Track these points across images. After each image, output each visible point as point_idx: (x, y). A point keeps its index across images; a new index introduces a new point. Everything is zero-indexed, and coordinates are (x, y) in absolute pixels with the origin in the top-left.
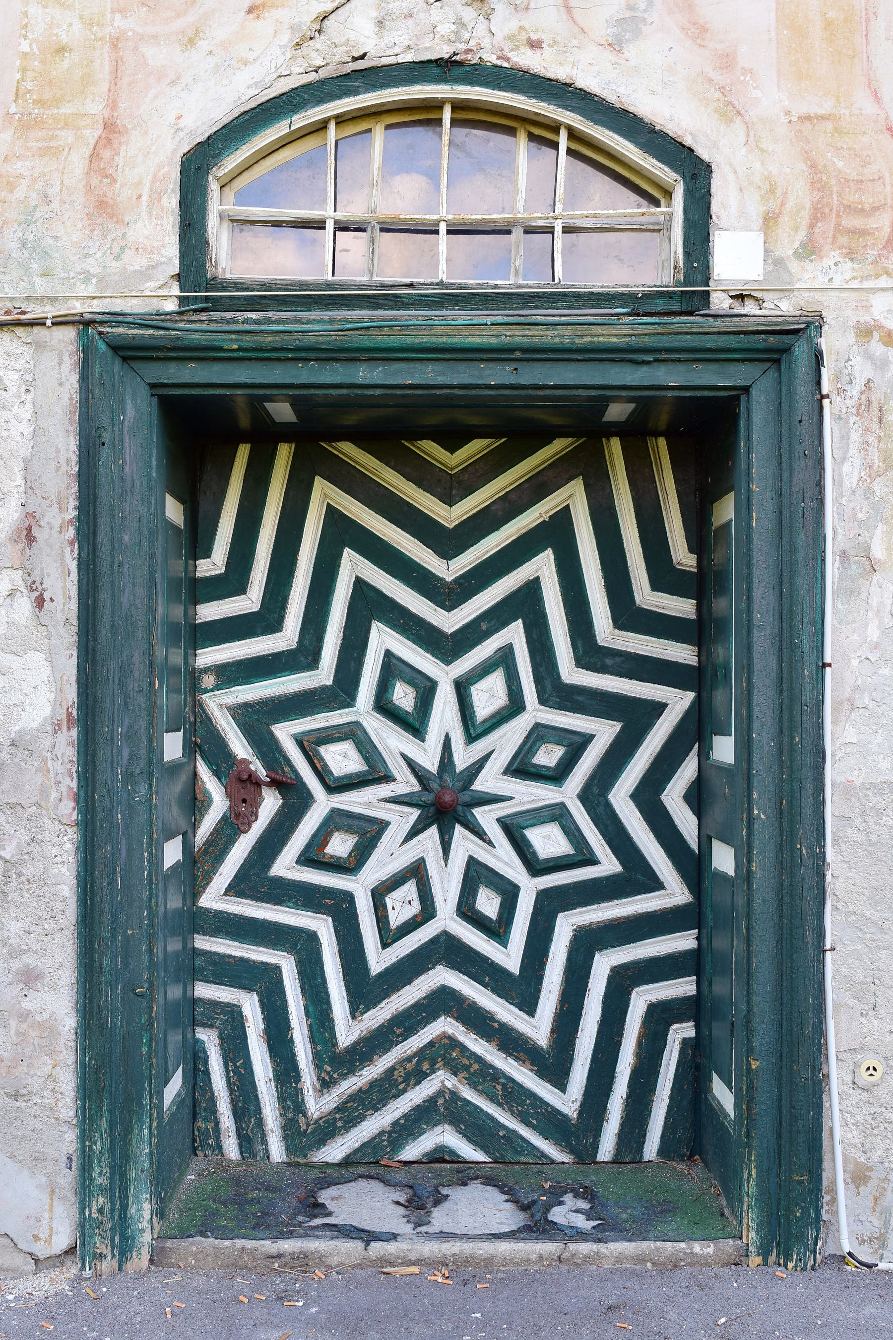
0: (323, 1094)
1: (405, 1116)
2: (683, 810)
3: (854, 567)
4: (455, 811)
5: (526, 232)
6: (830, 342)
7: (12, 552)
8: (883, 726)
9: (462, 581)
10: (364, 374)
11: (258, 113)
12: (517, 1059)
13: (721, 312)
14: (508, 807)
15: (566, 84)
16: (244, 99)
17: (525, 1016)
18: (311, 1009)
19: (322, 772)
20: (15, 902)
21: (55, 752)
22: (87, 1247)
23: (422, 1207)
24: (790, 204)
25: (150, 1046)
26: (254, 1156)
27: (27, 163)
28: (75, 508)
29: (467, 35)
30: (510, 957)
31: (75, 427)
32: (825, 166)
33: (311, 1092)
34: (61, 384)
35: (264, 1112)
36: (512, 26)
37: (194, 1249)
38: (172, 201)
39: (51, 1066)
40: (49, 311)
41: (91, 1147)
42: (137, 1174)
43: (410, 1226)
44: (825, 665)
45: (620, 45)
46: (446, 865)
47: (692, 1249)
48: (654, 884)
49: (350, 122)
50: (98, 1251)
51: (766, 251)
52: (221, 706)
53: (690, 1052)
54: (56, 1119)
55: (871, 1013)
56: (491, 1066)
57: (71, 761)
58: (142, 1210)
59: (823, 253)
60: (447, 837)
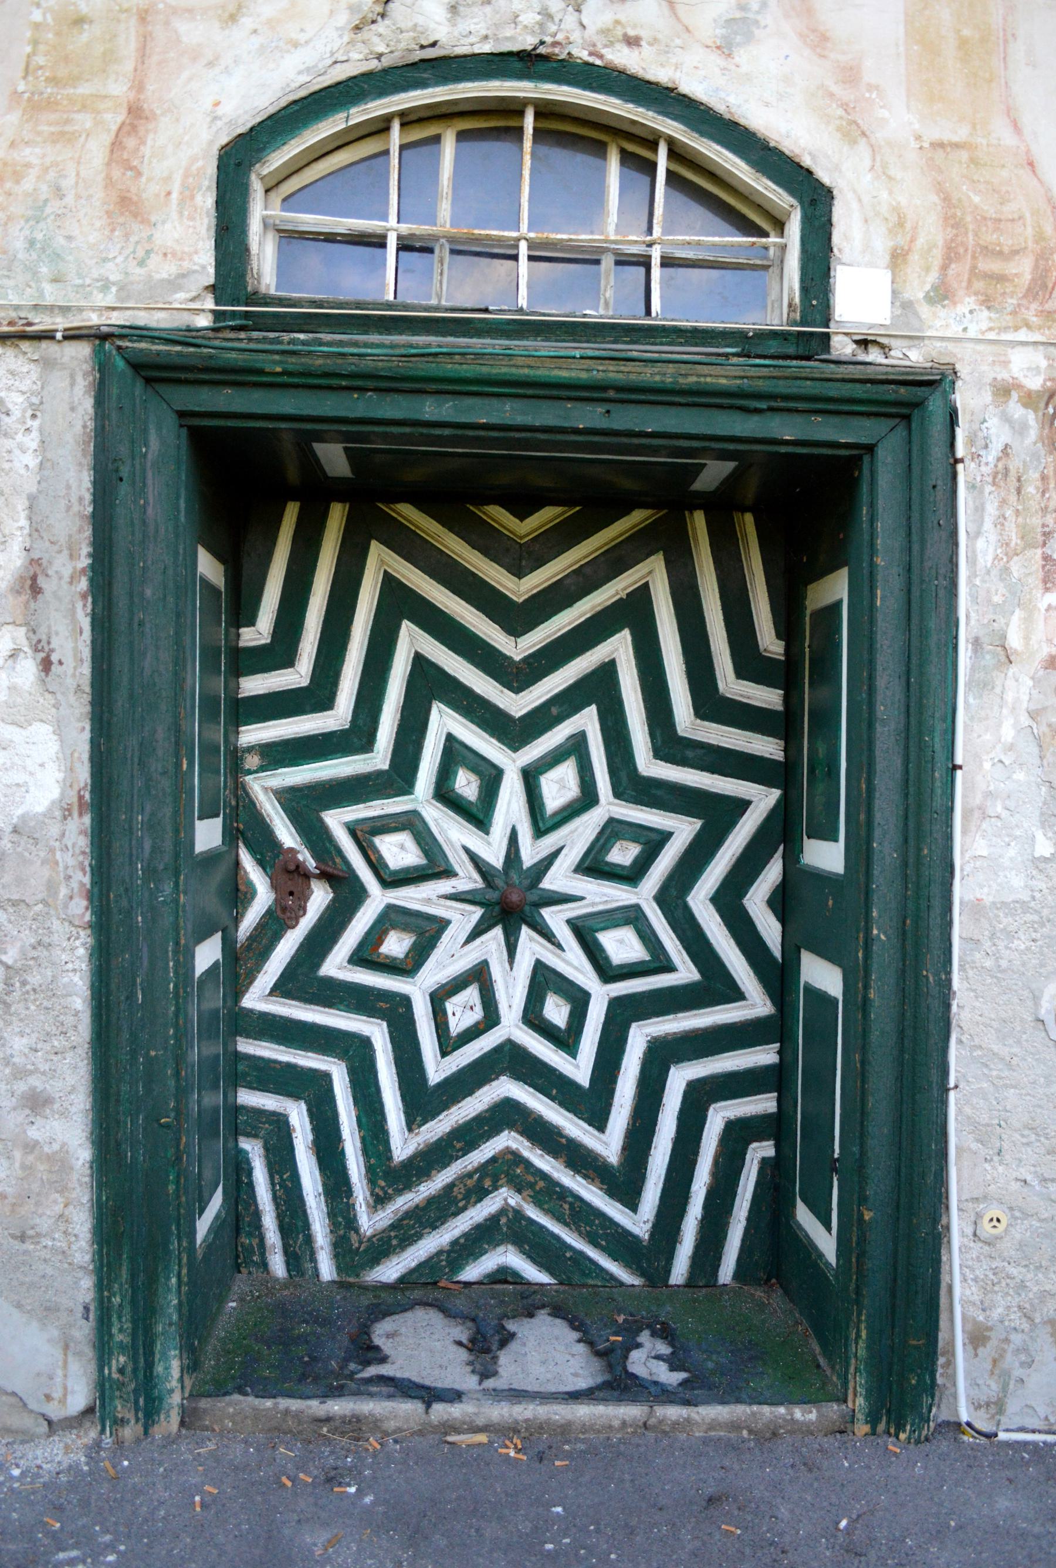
0: (376, 1211)
1: (465, 1235)
2: (766, 916)
3: (988, 657)
4: (522, 911)
5: (618, 263)
6: (964, 398)
7: (13, 604)
8: (1016, 838)
9: (531, 660)
10: (430, 409)
11: (309, 104)
12: (585, 1177)
13: (843, 358)
14: (578, 908)
15: (667, 88)
16: (294, 85)
17: (596, 1133)
18: (364, 1120)
19: (376, 865)
20: (19, 1014)
21: (65, 841)
22: (108, 1408)
23: (488, 1351)
24: (921, 241)
25: (178, 1183)
26: (303, 1275)
27: (37, 150)
28: (89, 555)
29: (553, 28)
30: (579, 1069)
31: (89, 460)
32: (960, 200)
33: (364, 1208)
34: (73, 409)
35: (313, 1227)
36: (606, 18)
37: (231, 1410)
38: (207, 200)
39: (62, 1205)
40: (61, 323)
41: (109, 1298)
42: (163, 1328)
43: (475, 1378)
44: (956, 767)
45: (730, 49)
46: (511, 969)
47: (792, 1415)
48: (733, 994)
49: (417, 125)
50: (120, 1416)
51: (894, 292)
52: (265, 789)
53: (769, 1172)
54: (70, 1264)
55: (996, 1158)
56: (558, 1184)
57: (83, 853)
58: (171, 1368)
59: (956, 299)
60: (512, 939)
